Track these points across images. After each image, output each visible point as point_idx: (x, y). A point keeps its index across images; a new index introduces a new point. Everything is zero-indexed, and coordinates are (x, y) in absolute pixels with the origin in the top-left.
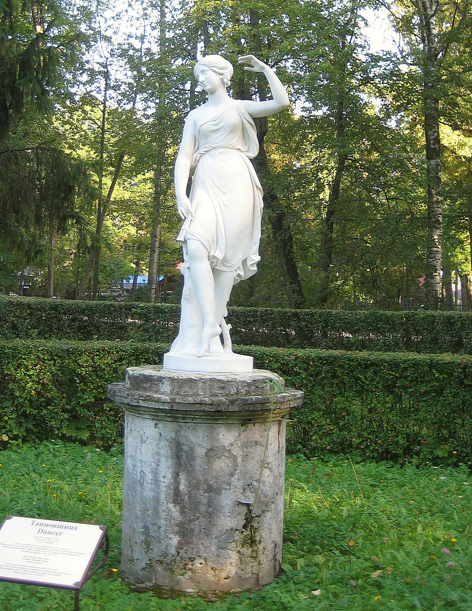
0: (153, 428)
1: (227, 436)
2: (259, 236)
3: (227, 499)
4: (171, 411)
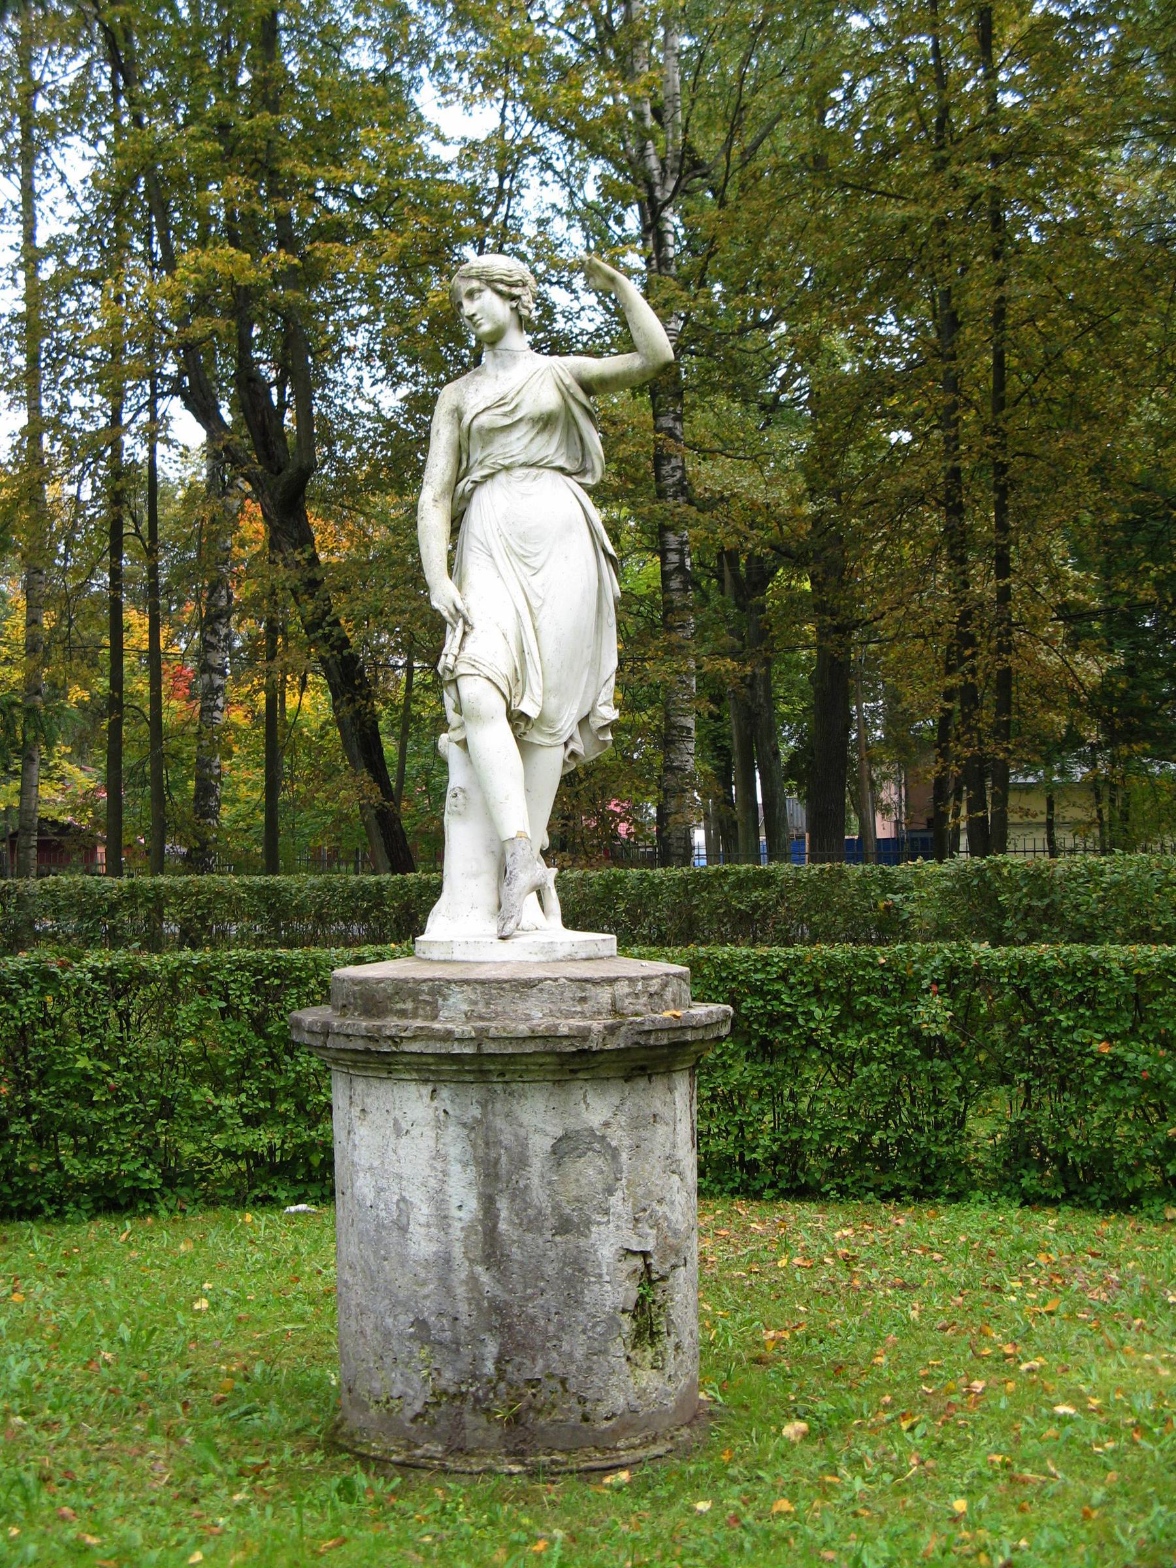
0: (427, 1100)
1: (597, 1109)
2: (614, 663)
3: (606, 1242)
4: (479, 1056)
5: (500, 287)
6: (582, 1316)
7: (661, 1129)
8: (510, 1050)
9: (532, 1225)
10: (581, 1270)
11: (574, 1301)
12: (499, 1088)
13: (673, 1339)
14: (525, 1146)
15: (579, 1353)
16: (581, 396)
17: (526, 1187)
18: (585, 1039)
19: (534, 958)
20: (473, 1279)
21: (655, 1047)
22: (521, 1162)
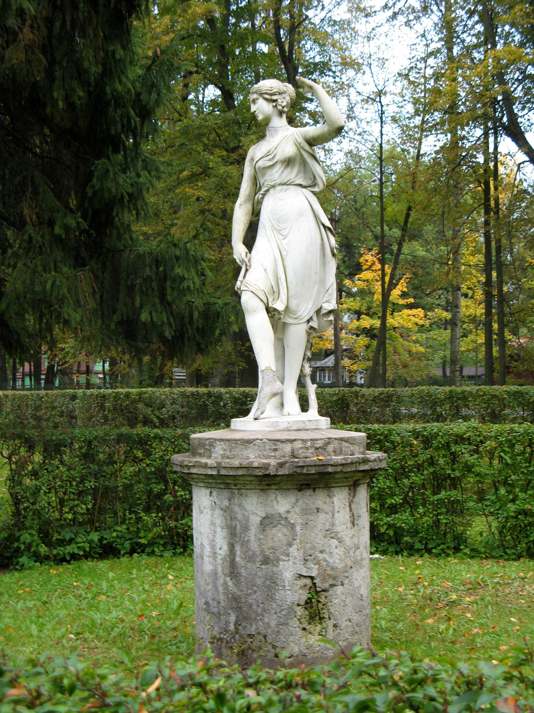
1: (283, 504)
3: (288, 570)
5: (266, 96)
6: (274, 606)
7: (322, 516)
8: (231, 474)
9: (251, 559)
10: (274, 583)
11: (270, 598)
12: (236, 491)
13: (332, 622)
14: (248, 520)
15: (273, 623)
16: (307, 147)
17: (248, 540)
18: (267, 469)
19: (268, 429)
20: (225, 583)
21: (307, 474)
22: (246, 528)
